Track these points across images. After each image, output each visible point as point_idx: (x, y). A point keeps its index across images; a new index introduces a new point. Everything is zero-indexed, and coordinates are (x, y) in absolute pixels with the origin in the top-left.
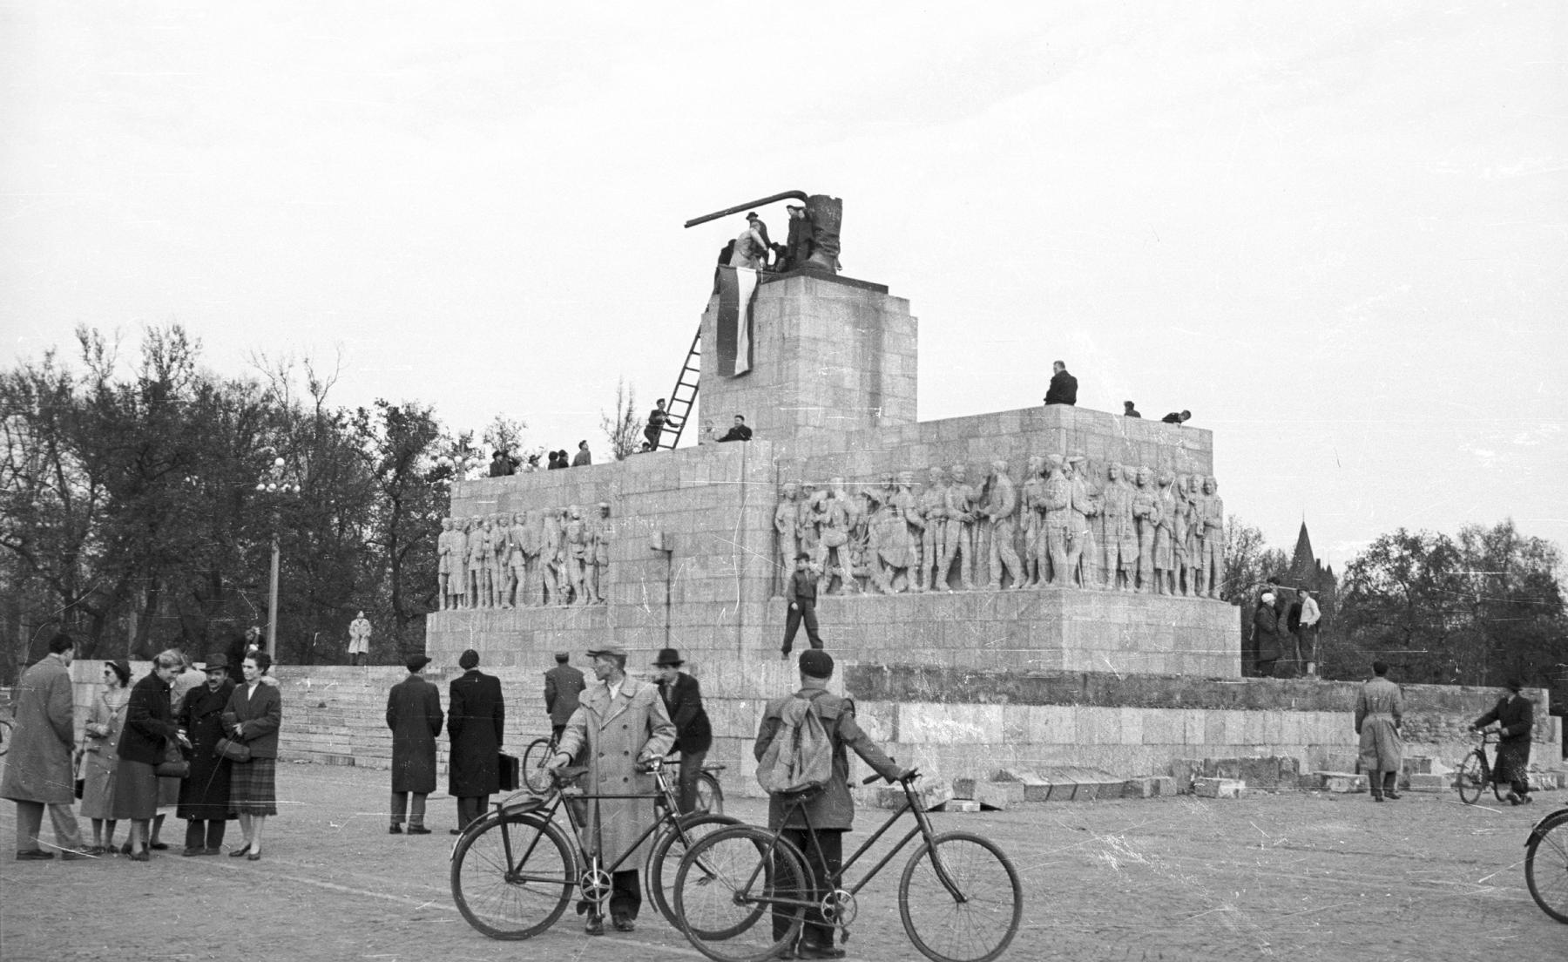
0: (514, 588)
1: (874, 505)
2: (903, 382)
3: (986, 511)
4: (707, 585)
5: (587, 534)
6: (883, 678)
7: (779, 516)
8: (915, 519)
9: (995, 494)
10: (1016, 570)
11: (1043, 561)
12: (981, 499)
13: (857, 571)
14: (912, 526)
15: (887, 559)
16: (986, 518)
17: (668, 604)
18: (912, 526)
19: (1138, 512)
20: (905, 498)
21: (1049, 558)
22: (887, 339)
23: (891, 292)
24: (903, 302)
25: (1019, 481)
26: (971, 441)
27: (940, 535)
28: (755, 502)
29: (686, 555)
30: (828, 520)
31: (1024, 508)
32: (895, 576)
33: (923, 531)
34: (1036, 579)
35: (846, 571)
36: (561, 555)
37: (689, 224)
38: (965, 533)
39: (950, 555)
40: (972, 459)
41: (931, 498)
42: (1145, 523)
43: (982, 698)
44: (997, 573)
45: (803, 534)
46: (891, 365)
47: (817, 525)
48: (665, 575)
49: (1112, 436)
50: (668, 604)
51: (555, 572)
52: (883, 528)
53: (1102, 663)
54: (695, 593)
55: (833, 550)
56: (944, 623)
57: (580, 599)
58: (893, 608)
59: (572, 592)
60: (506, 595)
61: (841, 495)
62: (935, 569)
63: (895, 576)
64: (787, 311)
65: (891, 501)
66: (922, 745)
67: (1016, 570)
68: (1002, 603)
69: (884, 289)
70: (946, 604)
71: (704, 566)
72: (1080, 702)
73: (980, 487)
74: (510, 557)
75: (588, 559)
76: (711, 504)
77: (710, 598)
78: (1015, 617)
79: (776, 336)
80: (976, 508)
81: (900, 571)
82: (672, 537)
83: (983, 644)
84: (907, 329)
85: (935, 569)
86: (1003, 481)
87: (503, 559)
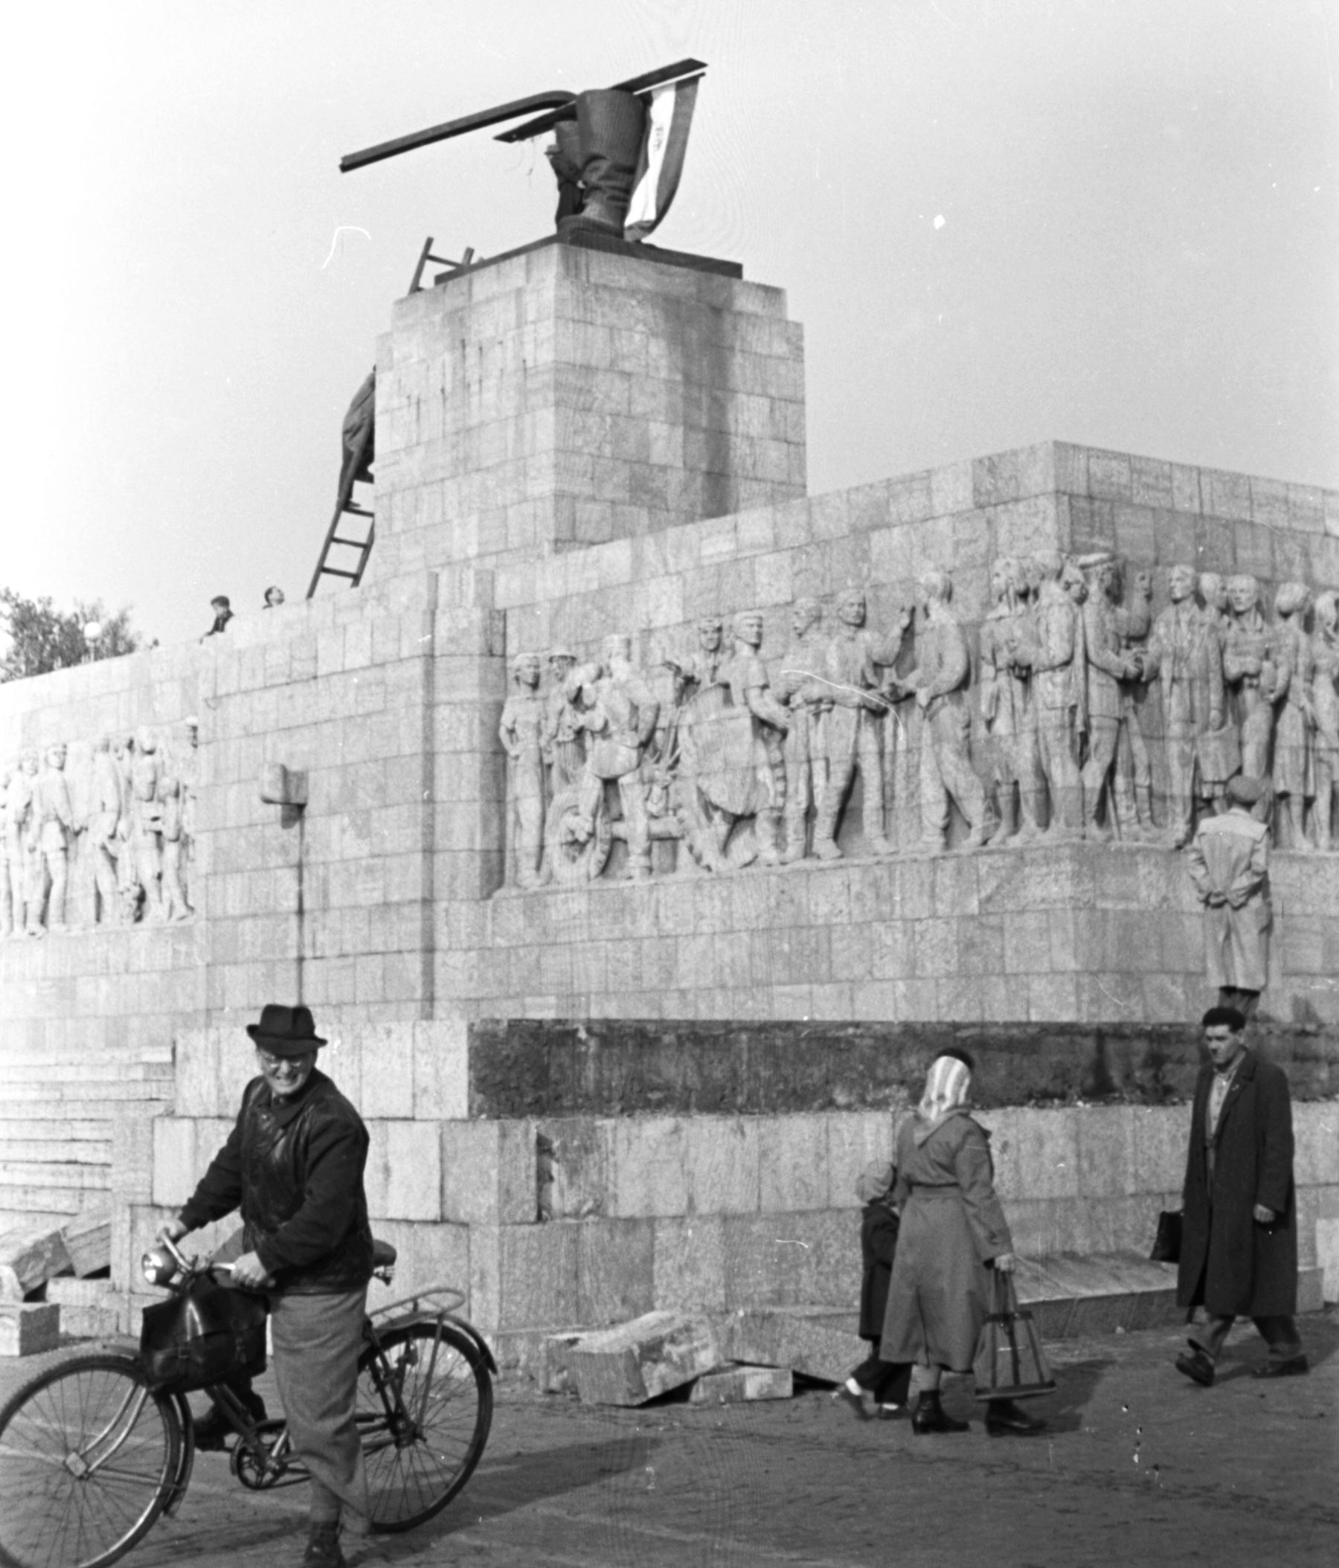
0: (47, 895)
1: (688, 684)
2: (774, 453)
3: (909, 683)
4: (370, 870)
5: (166, 784)
6: (578, 1058)
7: (506, 720)
8: (769, 707)
9: (924, 647)
10: (974, 808)
11: (1029, 786)
12: (899, 658)
13: (657, 828)
14: (762, 725)
15: (716, 798)
16: (910, 695)
17: (300, 912)
18: (762, 725)
19: (1234, 669)
20: (742, 667)
21: (1042, 775)
22: (740, 368)
23: (748, 275)
24: (773, 293)
25: (973, 616)
26: (875, 536)
27: (818, 740)
28: (456, 696)
29: (332, 812)
30: (598, 725)
31: (987, 671)
32: (731, 834)
33: (784, 733)
34: (1016, 825)
35: (635, 827)
36: (122, 827)
37: (350, 164)
38: (868, 737)
39: (839, 781)
40: (879, 576)
41: (793, 667)
42: (1249, 695)
43: (841, 1098)
44: (935, 814)
45: (554, 756)
46: (748, 416)
47: (580, 733)
48: (294, 858)
49: (1172, 511)
50: (300, 912)
51: (113, 860)
52: (706, 732)
53: (1163, 996)
54: (348, 886)
55: (610, 784)
56: (829, 927)
57: (155, 909)
58: (727, 901)
59: (141, 898)
60: (35, 909)
61: (621, 669)
62: (810, 814)
63: (731, 834)
64: (531, 316)
65: (722, 675)
66: (679, 1220)
67: (974, 808)
68: (945, 877)
69: (734, 270)
70: (831, 893)
71: (363, 831)
72: (1089, 1095)
73: (896, 631)
74: (39, 837)
75: (169, 832)
76: (374, 703)
77: (377, 896)
78: (973, 906)
79: (511, 365)
80: (890, 675)
81: (739, 821)
82: (302, 777)
83: (912, 970)
84: (780, 348)
85: (810, 814)
86: (940, 614)
87: (28, 838)
